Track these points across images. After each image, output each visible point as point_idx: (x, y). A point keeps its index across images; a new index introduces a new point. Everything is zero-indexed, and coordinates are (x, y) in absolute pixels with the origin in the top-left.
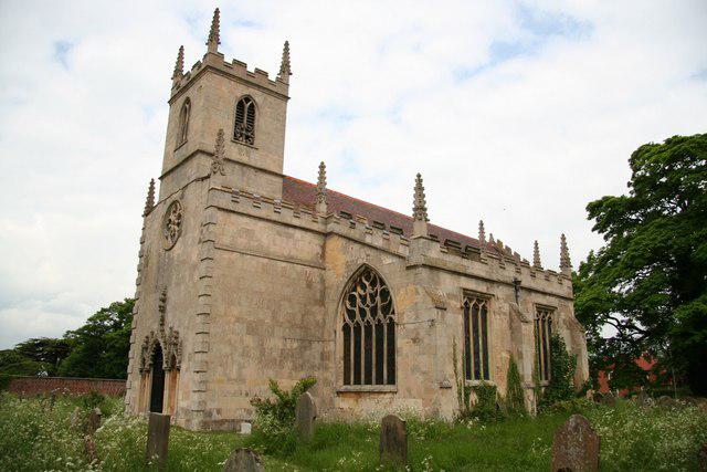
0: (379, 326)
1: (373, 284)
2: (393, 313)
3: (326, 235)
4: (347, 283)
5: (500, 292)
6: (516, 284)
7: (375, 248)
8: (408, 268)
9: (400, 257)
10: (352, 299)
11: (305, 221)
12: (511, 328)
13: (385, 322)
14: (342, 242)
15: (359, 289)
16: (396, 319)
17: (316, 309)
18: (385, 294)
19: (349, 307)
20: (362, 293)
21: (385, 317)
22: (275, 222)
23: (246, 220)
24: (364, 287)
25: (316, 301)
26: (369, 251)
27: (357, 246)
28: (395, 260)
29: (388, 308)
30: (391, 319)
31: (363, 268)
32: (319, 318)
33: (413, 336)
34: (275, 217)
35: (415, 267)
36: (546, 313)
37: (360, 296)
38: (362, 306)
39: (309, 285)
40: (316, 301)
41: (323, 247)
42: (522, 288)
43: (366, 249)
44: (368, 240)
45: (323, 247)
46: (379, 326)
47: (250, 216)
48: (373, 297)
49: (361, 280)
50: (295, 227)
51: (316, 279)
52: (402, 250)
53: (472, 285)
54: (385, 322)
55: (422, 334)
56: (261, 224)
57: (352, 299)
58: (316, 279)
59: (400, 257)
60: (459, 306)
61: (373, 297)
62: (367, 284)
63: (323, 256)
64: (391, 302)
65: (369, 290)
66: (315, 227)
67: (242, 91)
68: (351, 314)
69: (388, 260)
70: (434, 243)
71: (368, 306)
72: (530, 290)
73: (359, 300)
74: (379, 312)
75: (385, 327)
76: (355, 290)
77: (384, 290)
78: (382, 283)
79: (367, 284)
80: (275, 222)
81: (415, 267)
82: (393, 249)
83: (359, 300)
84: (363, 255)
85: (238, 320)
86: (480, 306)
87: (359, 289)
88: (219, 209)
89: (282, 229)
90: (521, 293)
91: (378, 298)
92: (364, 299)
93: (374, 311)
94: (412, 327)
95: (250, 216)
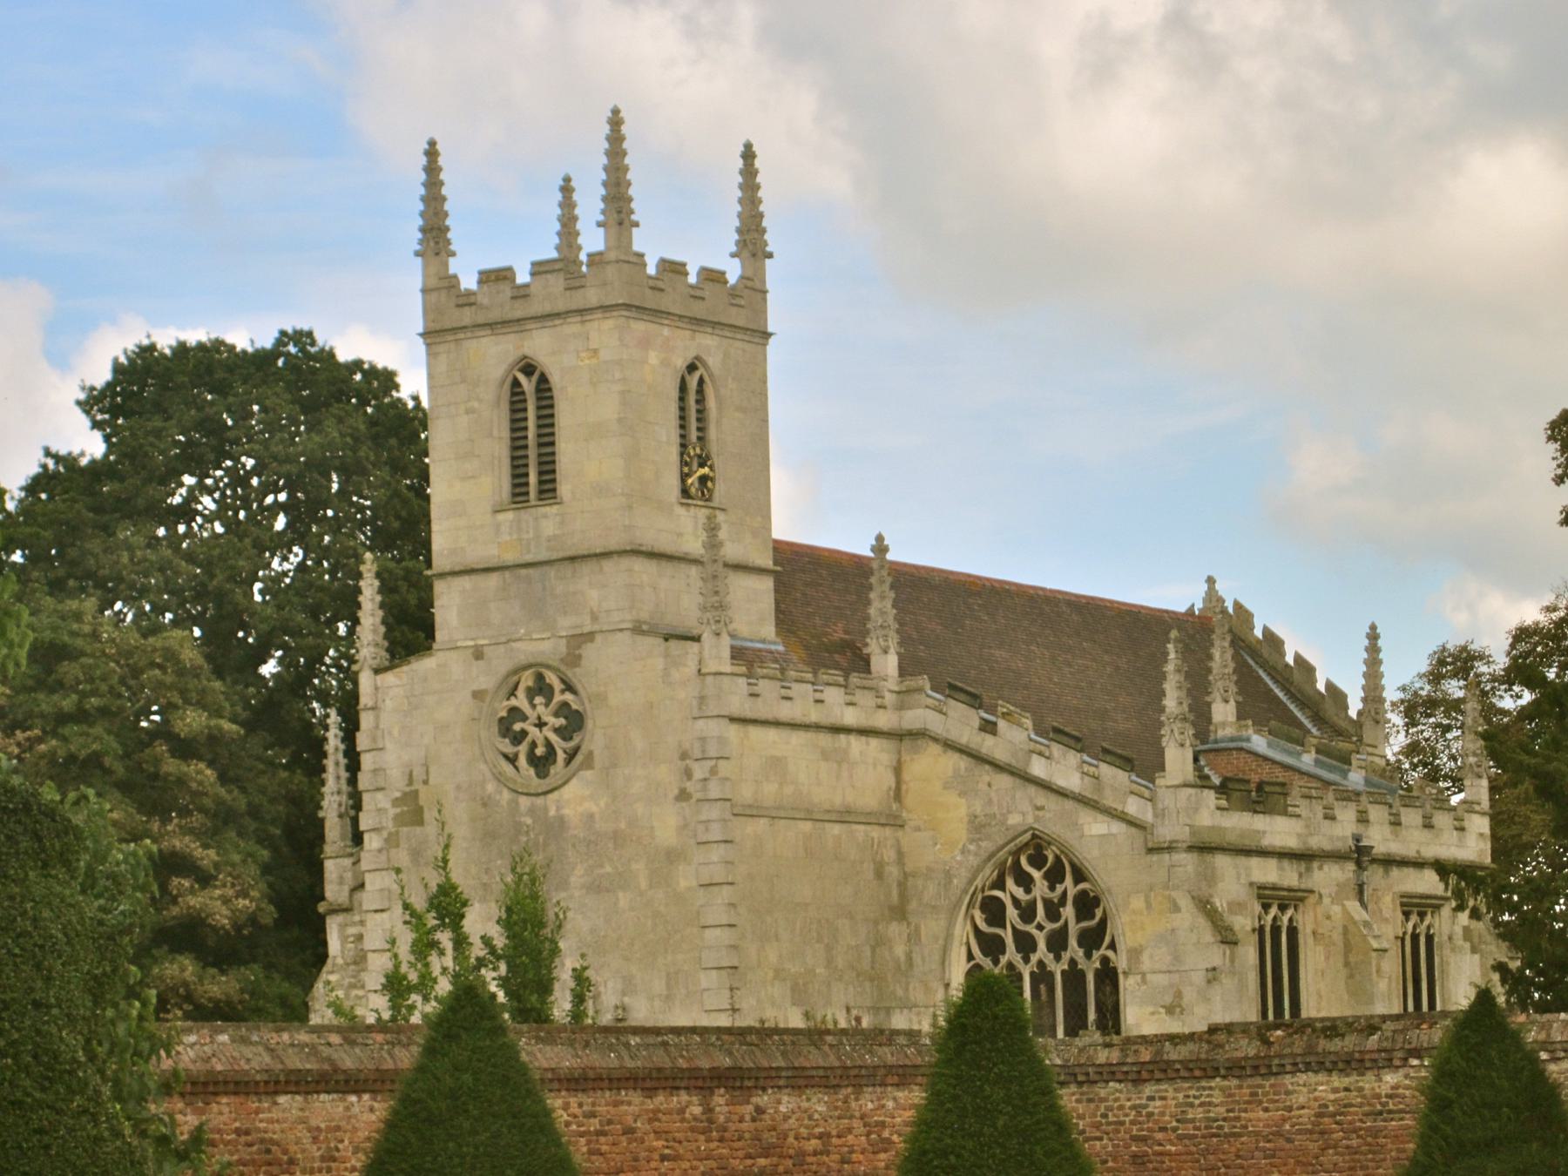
0: (1074, 977)
1: (1054, 877)
2: (1112, 946)
3: (898, 736)
4: (979, 869)
5: (1330, 877)
6: (1360, 855)
7: (1062, 793)
8: (1150, 851)
9: (1131, 822)
10: (994, 912)
11: (837, 705)
12: (1347, 964)
13: (1090, 968)
14: (953, 763)
15: (1010, 883)
16: (1121, 962)
17: (895, 930)
18: (1087, 904)
19: (983, 926)
20: (1019, 892)
21: (1088, 955)
22: (817, 727)
23: (772, 734)
24: (1025, 881)
25: (892, 909)
26: (1041, 798)
27: (1004, 781)
28: (1117, 828)
29: (1093, 939)
30: (1105, 960)
31: (1028, 836)
32: (900, 951)
33: (1168, 999)
34: (814, 716)
35: (1170, 848)
36: (1422, 915)
37: (1016, 902)
38: (1021, 926)
39: (879, 874)
40: (892, 909)
41: (898, 770)
42: (1374, 861)
43: (1032, 790)
44: (1038, 768)
45: (898, 770)
46: (1074, 977)
47: (777, 724)
48: (1053, 911)
49: (1017, 863)
50: (847, 730)
51: (889, 855)
52: (1133, 807)
53: (1268, 872)
54: (1090, 968)
55: (1189, 995)
56: (797, 738)
57: (994, 912)
58: (889, 855)
59: (1131, 822)
60: (1249, 928)
61: (1053, 911)
62: (1037, 875)
63: (898, 794)
64: (1103, 922)
65: (1041, 888)
66: (883, 720)
67: (683, 345)
68: (992, 946)
69: (1096, 826)
70: (1206, 791)
71: (1040, 927)
72: (1389, 862)
73: (1012, 913)
74: (1073, 942)
75: (1090, 978)
76: (1000, 884)
77: (1084, 893)
78: (1079, 876)
79: (1037, 875)
80: (817, 727)
81: (1170, 848)
82: (1109, 801)
83: (1012, 913)
84: (1027, 807)
85: (779, 974)
86: (1285, 919)
87: (1010, 883)
88: (733, 720)
89: (825, 739)
90: (1374, 875)
91: (1068, 912)
92: (1027, 913)
93: (1057, 943)
94: (1162, 980)
95: (777, 724)
